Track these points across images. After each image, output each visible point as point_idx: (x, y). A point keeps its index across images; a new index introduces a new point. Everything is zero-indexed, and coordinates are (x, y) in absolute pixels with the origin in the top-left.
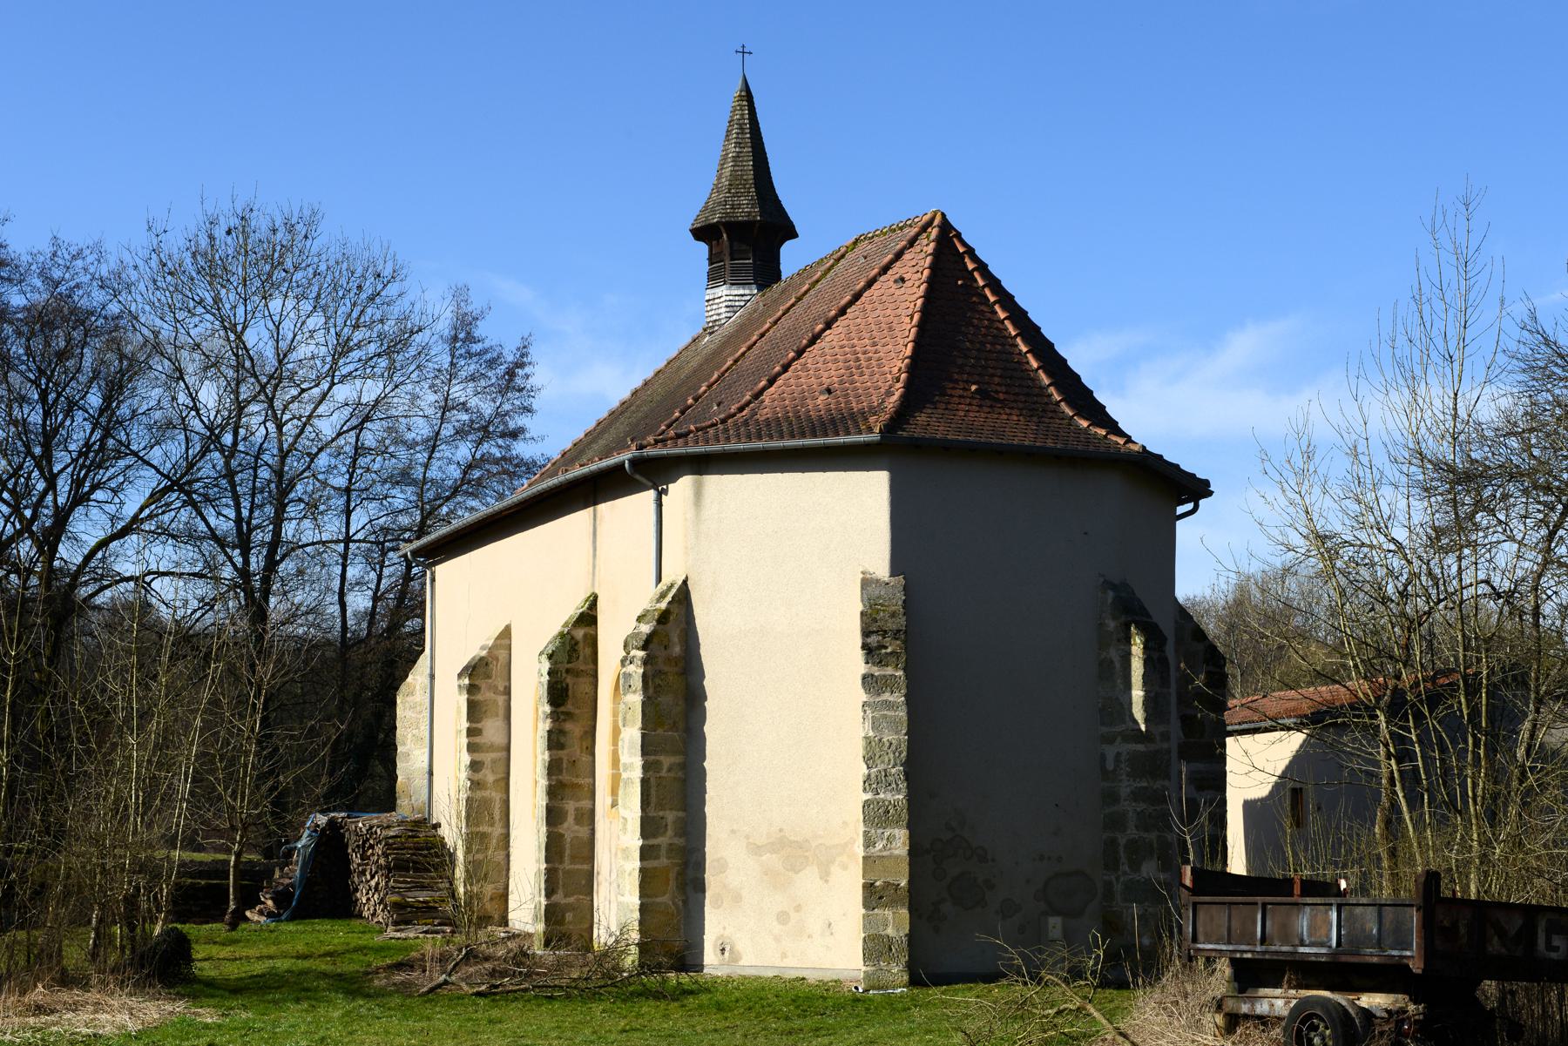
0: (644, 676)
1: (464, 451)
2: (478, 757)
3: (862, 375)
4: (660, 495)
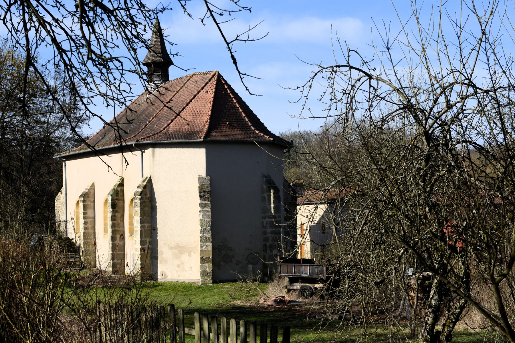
0: (140, 203)
2: (86, 220)
3: (197, 120)
4: (142, 152)
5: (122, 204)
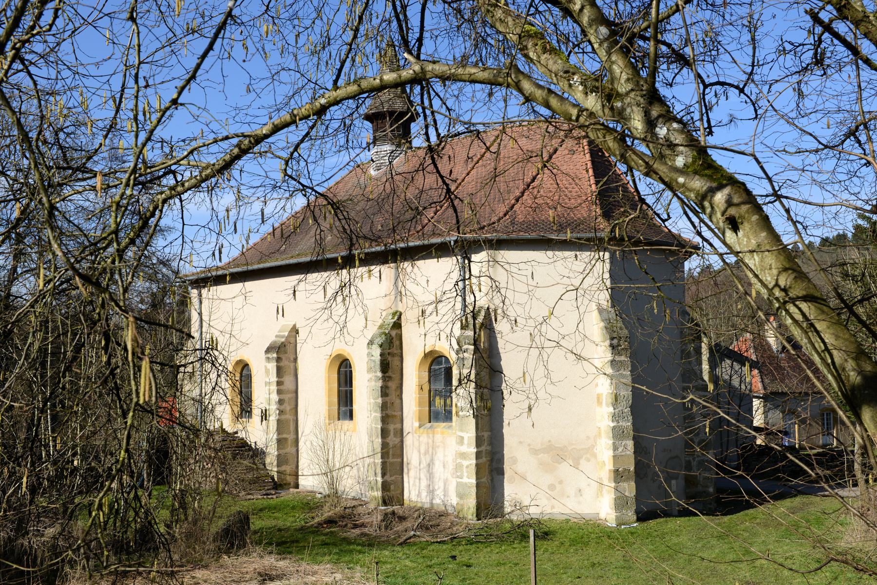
2: (283, 396)
5: (398, 363)
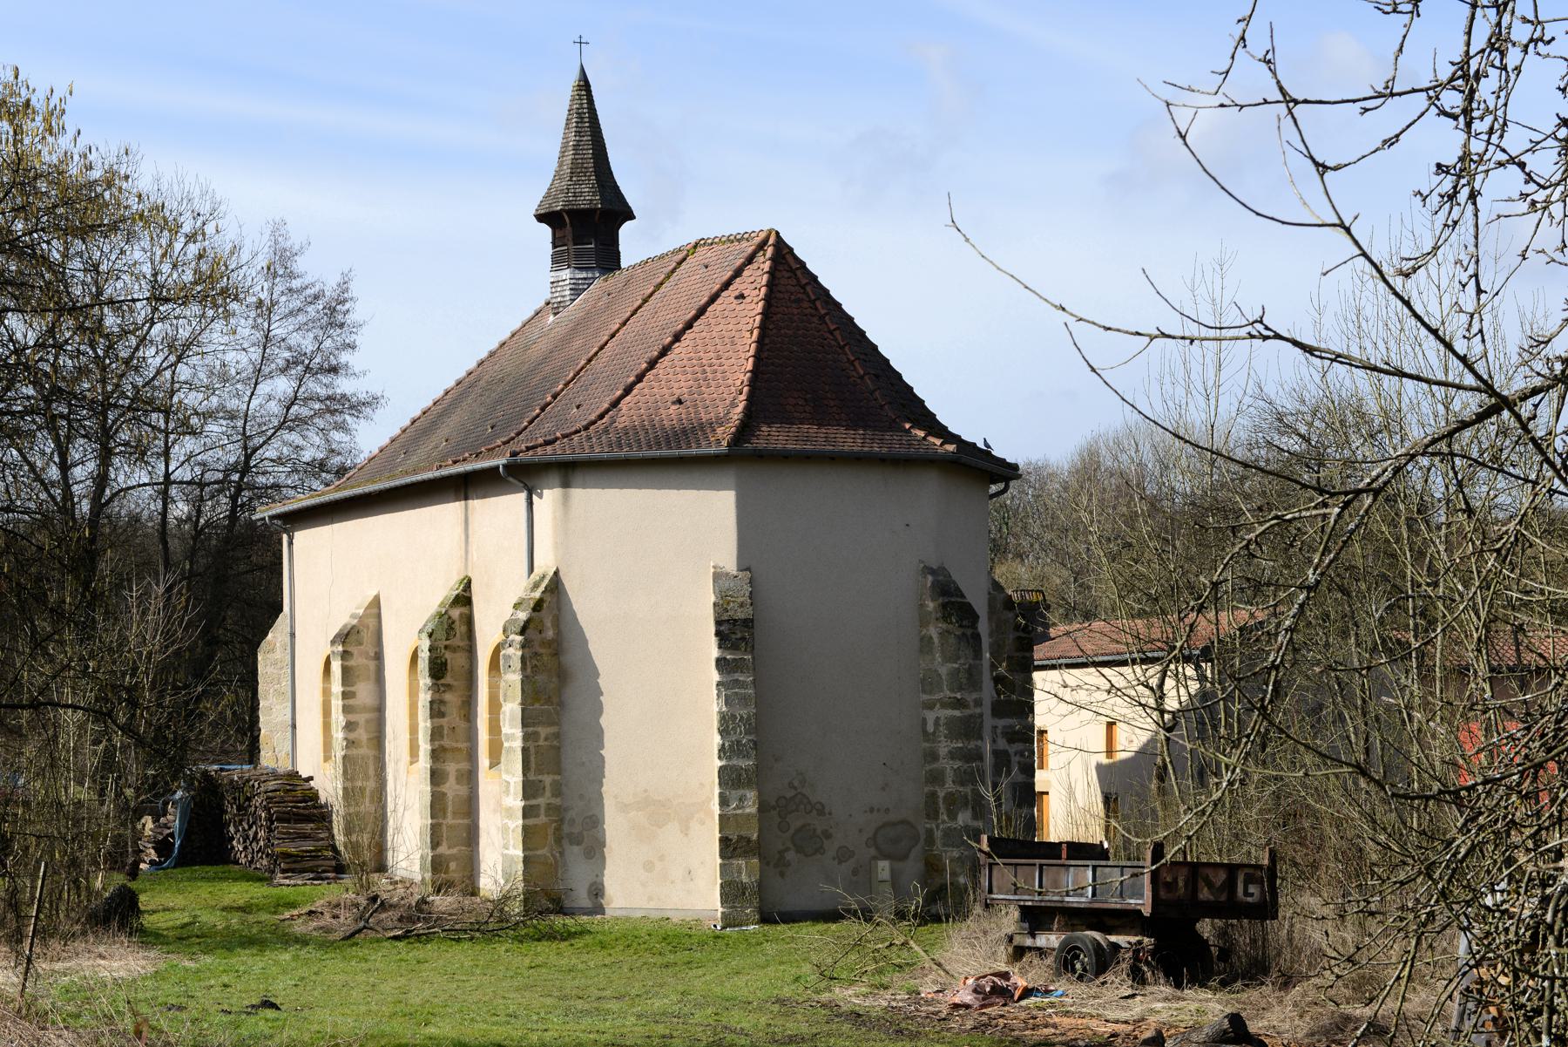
0: (523, 658)
1: (283, 386)
2: (353, 717)
3: (709, 386)
